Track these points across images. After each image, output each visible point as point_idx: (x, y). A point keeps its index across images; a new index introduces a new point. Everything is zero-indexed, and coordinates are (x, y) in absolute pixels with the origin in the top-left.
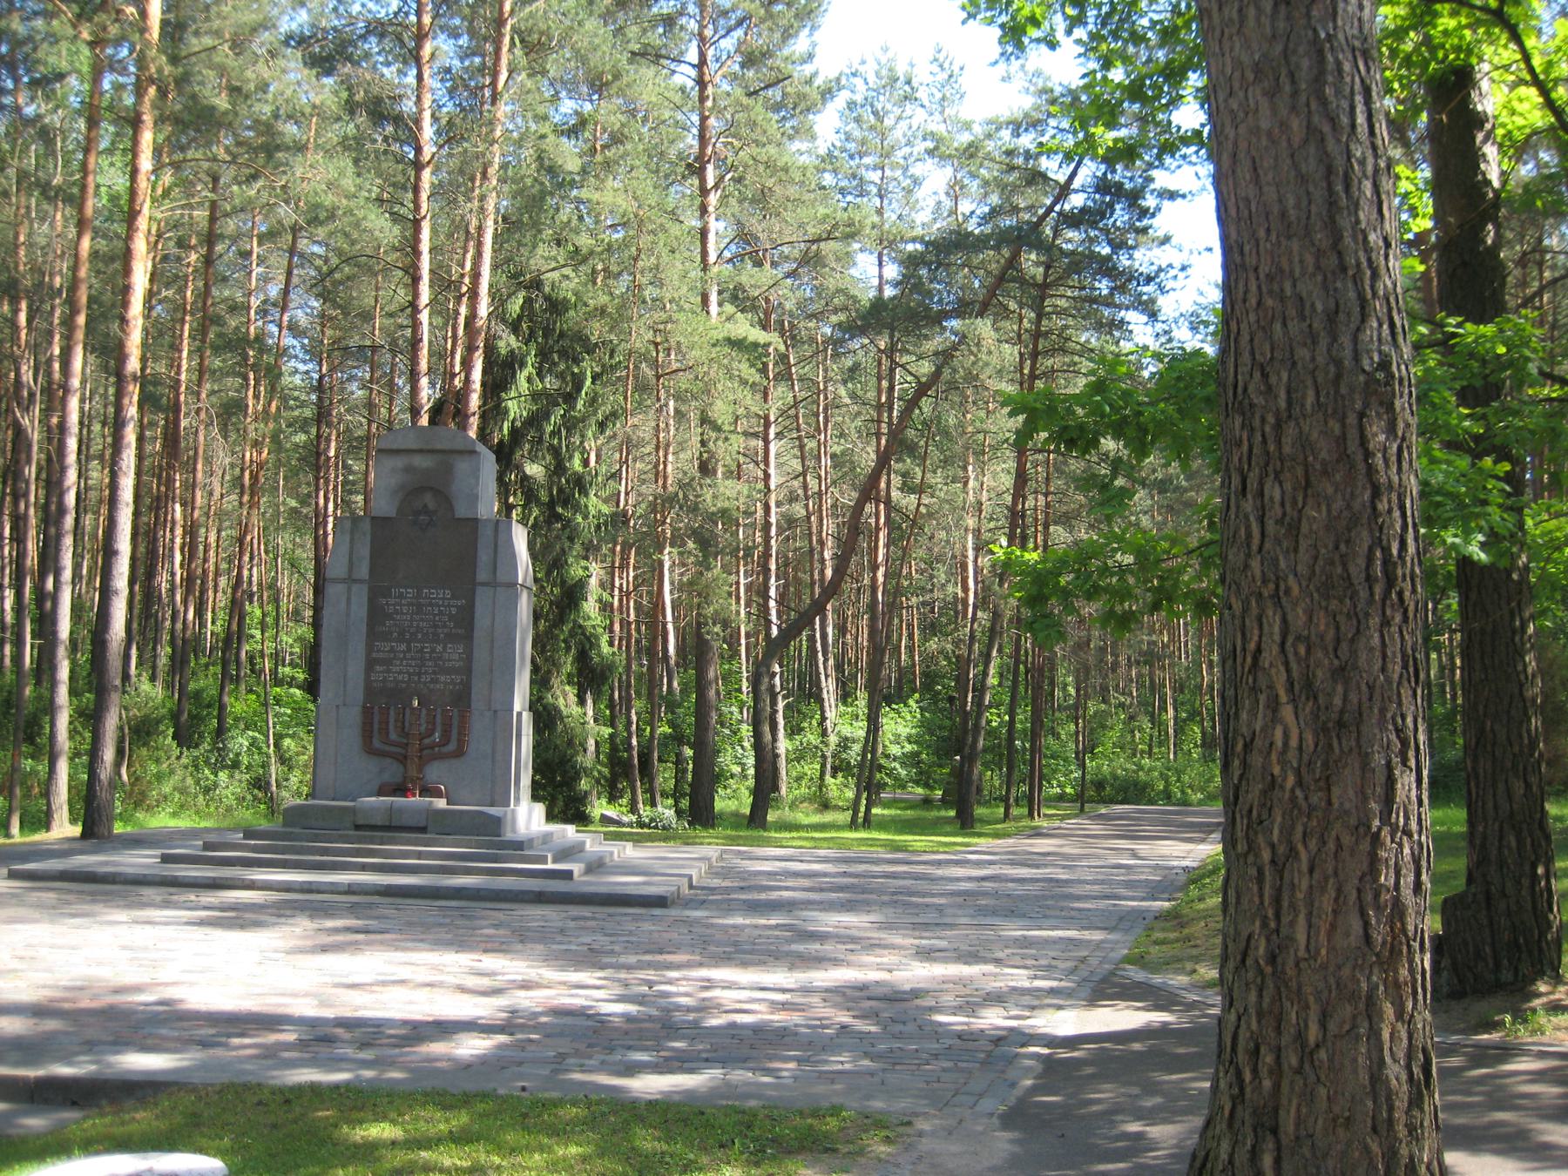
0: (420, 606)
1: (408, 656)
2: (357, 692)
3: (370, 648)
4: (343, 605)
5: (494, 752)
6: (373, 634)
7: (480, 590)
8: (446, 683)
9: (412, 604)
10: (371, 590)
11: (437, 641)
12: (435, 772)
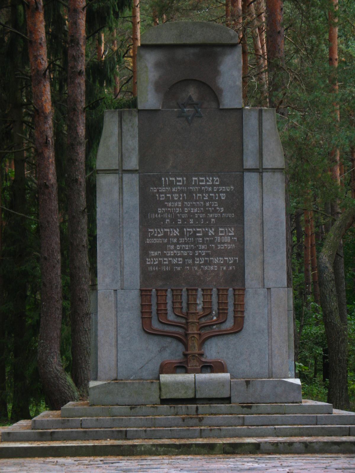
0: (190, 193)
1: (181, 240)
2: (134, 279)
3: (144, 235)
4: (116, 195)
5: (269, 327)
6: (146, 222)
7: (247, 175)
8: (219, 265)
9: (182, 192)
10: (141, 180)
11: (210, 226)
12: (213, 350)
